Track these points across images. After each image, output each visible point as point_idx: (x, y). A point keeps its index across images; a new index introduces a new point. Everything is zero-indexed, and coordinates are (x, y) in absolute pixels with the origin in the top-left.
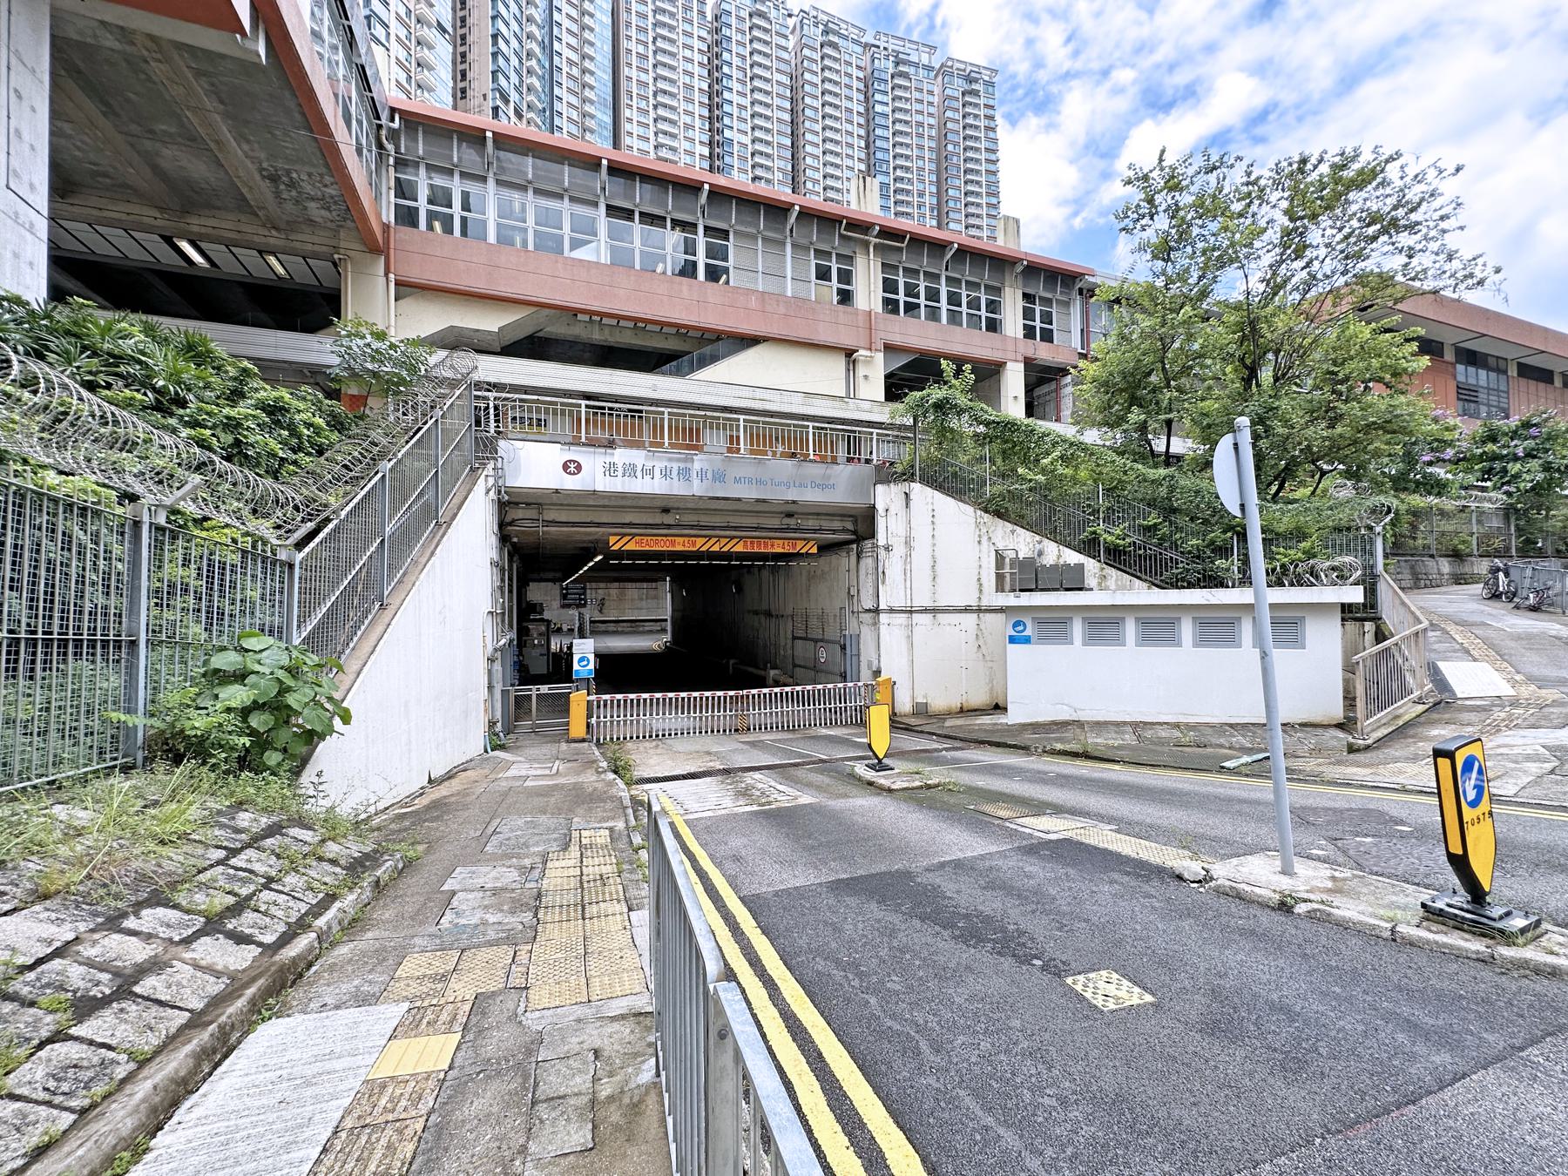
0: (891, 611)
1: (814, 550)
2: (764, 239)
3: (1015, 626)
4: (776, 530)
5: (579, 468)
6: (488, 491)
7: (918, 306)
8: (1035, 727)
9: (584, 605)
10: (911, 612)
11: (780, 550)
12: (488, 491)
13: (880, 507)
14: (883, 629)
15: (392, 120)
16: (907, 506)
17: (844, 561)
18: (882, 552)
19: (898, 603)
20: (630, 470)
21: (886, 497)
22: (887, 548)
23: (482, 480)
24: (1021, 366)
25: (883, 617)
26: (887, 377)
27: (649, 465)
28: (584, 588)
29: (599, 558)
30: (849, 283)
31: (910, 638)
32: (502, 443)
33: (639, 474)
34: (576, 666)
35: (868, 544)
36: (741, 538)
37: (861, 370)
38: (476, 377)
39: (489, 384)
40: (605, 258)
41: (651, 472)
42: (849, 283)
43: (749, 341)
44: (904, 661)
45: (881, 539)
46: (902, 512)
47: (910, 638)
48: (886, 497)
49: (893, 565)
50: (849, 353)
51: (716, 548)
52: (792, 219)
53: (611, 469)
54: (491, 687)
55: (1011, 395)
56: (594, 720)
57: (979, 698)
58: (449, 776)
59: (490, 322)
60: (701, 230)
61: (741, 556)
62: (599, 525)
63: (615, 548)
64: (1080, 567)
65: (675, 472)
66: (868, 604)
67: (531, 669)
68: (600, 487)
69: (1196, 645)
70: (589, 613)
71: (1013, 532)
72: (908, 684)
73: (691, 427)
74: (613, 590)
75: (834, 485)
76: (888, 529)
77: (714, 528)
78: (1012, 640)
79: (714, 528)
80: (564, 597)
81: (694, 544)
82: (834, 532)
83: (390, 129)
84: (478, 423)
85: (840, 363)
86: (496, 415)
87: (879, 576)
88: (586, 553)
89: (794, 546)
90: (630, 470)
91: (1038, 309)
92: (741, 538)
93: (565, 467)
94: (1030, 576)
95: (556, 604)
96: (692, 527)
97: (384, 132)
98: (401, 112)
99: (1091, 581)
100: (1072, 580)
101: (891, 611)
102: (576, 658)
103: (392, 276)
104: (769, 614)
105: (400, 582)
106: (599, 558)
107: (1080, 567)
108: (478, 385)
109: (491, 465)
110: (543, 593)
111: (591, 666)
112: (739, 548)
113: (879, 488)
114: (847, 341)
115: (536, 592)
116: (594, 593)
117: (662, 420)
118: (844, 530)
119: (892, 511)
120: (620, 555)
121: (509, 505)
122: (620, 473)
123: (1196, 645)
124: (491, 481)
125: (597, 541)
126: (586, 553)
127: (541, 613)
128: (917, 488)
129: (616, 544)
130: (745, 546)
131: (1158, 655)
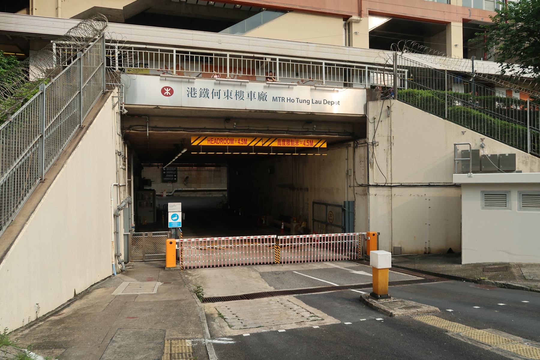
0: (377, 186)
1: (325, 146)
5: (172, 92)
6: (114, 107)
8: (485, 268)
9: (175, 181)
10: (391, 187)
12: (114, 107)
14: (372, 198)
17: (344, 153)
18: (370, 147)
19: (381, 182)
20: (205, 93)
23: (109, 100)
24: (461, 25)
25: (372, 190)
27: (216, 90)
28: (176, 171)
29: (185, 151)
32: (123, 76)
33: (210, 95)
34: (170, 220)
35: (362, 141)
37: (355, 28)
43: (284, 10)
48: (376, 109)
49: (379, 154)
50: (346, 18)
53: (192, 93)
54: (116, 233)
55: (453, 44)
57: (438, 243)
58: (87, 292)
61: (276, 149)
63: (195, 144)
64: (513, 157)
65: (233, 94)
66: (361, 181)
67: (147, 216)
69: (520, 209)
70: (179, 186)
71: (463, 133)
74: (193, 172)
75: (344, 101)
80: (164, 176)
84: (108, 64)
85: (341, 22)
86: (120, 61)
87: (368, 163)
88: (178, 148)
90: (205, 93)
93: (163, 91)
94: (473, 161)
95: (159, 180)
99: (519, 165)
100: (506, 164)
101: (377, 186)
102: (170, 215)
104: (292, 187)
105: (54, 164)
106: (185, 151)
107: (513, 157)
109: (116, 90)
110: (151, 173)
111: (180, 220)
115: (149, 173)
116: (182, 172)
120: (198, 148)
121: (132, 120)
123: (520, 209)
124: (116, 100)
125: (184, 140)
126: (178, 148)
127: (150, 185)
128: (396, 104)
131: (496, 214)
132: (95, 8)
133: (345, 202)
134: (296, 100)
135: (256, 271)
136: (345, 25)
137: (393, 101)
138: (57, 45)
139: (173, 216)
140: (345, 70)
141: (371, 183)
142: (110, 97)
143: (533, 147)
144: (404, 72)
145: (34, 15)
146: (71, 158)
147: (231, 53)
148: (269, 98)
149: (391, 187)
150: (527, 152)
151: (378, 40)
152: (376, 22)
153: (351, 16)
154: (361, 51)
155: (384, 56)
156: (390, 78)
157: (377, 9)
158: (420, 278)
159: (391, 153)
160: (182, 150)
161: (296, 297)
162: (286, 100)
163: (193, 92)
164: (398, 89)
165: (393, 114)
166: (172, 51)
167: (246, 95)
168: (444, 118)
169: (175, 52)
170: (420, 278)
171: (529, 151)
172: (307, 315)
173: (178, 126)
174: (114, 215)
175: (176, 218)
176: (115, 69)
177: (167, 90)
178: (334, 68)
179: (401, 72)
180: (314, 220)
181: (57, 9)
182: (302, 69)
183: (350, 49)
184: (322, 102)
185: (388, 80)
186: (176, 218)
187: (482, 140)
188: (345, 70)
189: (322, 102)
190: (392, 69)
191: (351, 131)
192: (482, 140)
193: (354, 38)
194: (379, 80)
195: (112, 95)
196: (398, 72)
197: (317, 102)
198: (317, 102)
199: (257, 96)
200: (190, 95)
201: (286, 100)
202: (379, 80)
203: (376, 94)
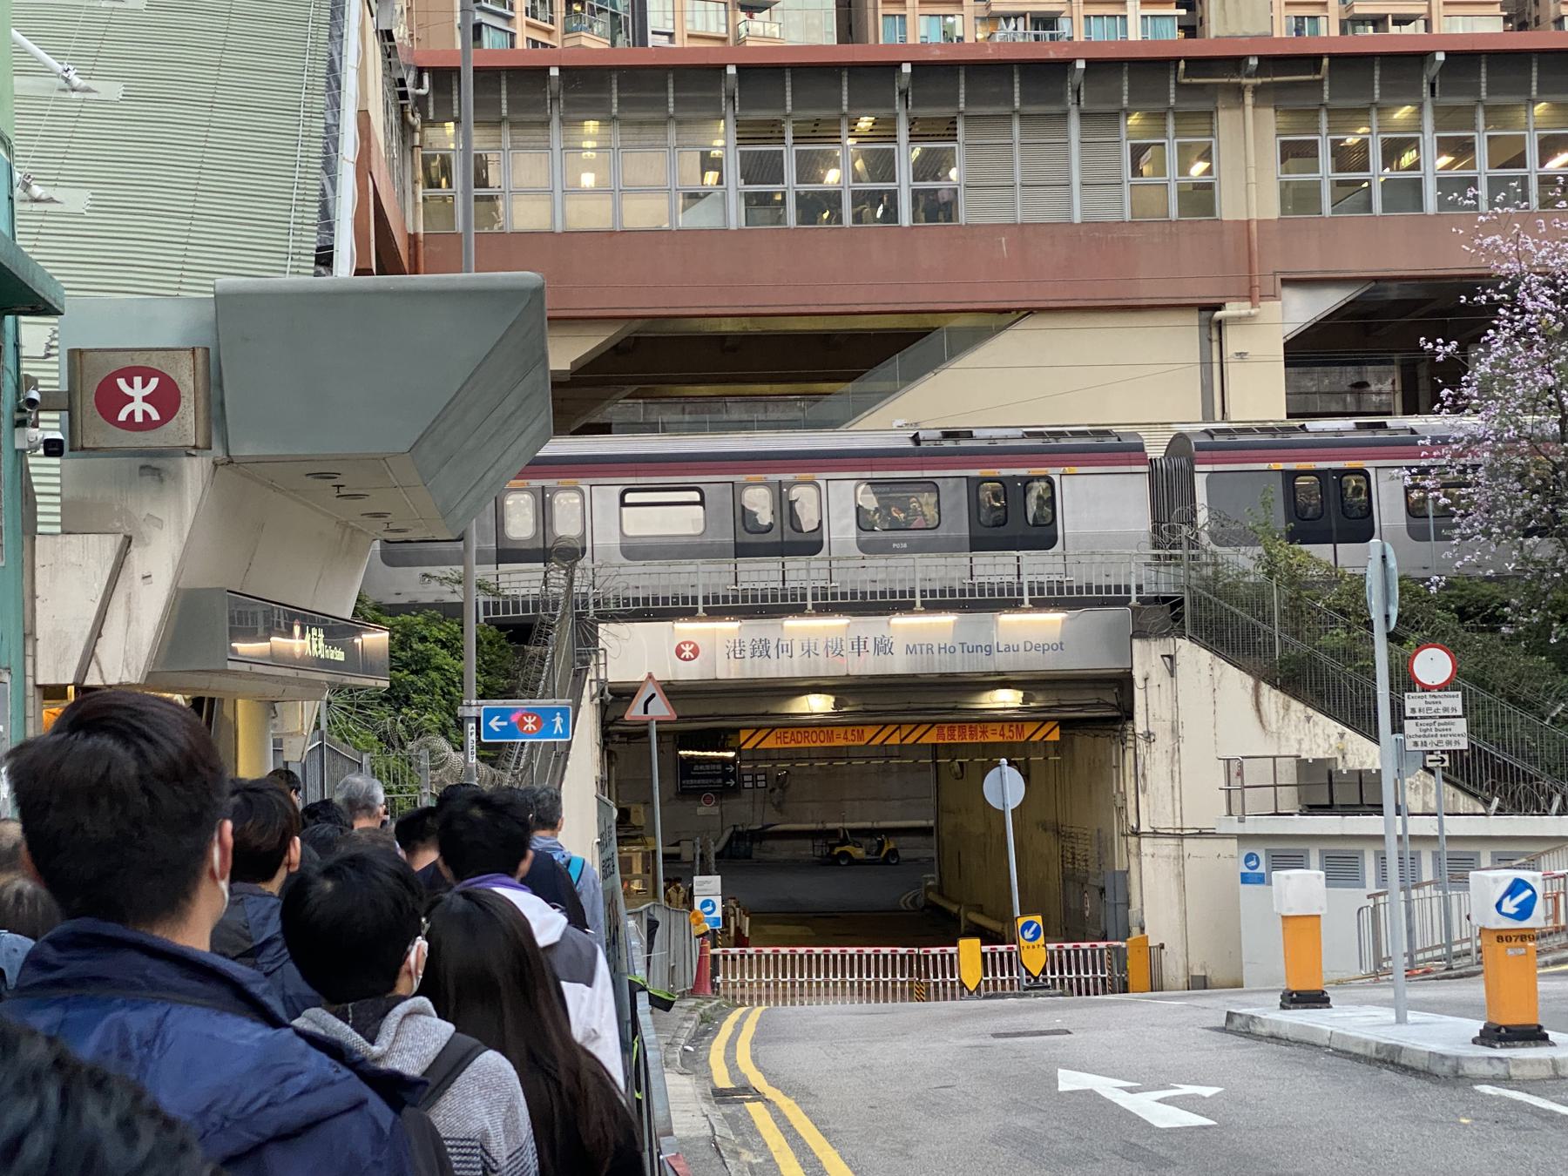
0: (1155, 834)
1: (1055, 736)
2: (1021, 116)
3: (1246, 861)
10: (1182, 837)
13: (1138, 675)
15: (419, 84)
18: (1141, 743)
19: (1165, 823)
21: (1146, 659)
26: (1285, 345)
31: (1181, 876)
33: (773, 652)
36: (933, 723)
37: (1234, 340)
43: (1031, 311)
44: (1175, 914)
45: (1140, 724)
46: (1166, 681)
47: (1181, 876)
48: (1146, 659)
51: (895, 740)
52: (1077, 78)
56: (719, 979)
62: (724, 717)
68: (722, 674)
72: (1180, 950)
76: (1149, 706)
78: (1245, 879)
79: (887, 713)
83: (418, 97)
92: (933, 723)
97: (410, 102)
98: (429, 69)
101: (1155, 834)
112: (931, 738)
113: (1136, 643)
114: (1204, 292)
118: (1099, 705)
119: (1153, 682)
122: (748, 654)
134: (959, 648)
137: (1179, 641)
139: (705, 904)
146: (228, 421)
147: (802, 573)
149: (1182, 837)
152: (1303, 310)
157: (1312, 266)
165: (1179, 670)
173: (710, 712)
175: (709, 909)
177: (687, 649)
186: (709, 909)
187: (1342, 736)
192: (1342, 736)
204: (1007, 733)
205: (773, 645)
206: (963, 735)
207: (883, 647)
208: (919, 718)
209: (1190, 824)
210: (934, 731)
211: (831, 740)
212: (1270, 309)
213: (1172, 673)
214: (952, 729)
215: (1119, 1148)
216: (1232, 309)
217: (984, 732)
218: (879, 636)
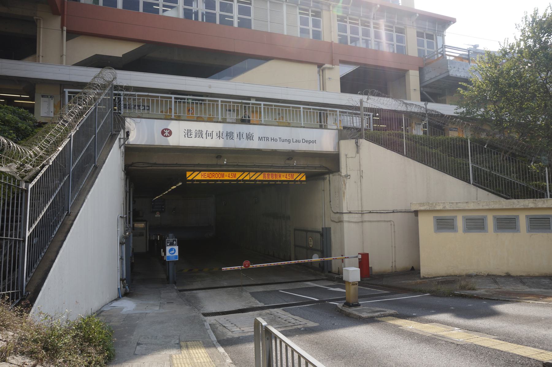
4: (282, 167)
7: (358, 39)
11: (284, 179)
12: (120, 147)
16: (358, 152)
19: (354, 207)
22: (347, 176)
23: (117, 142)
26: (341, 78)
30: (319, 27)
33: (204, 136)
37: (327, 74)
38: (115, 83)
39: (122, 87)
40: (181, 15)
41: (211, 135)
42: (319, 27)
43: (267, 59)
45: (343, 172)
48: (347, 147)
50: (320, 66)
55: (412, 88)
59: (118, 50)
60: (310, 11)
63: (190, 178)
69: (495, 231)
73: (245, 110)
75: (324, 140)
76: (347, 165)
77: (246, 166)
81: (235, 176)
82: (315, 168)
85: (315, 69)
89: (292, 177)
91: (348, 26)
96: (234, 166)
103: (65, 28)
106: (180, 184)
108: (116, 88)
117: (260, 108)
122: (193, 136)
128: (364, 143)
129: (191, 176)
130: (264, 177)
132: (97, 55)
133: (322, 228)
135: (246, 291)
136: (319, 72)
138: (69, 92)
140: (320, 113)
141: (345, 211)
142: (118, 139)
143: (475, 179)
144: (369, 115)
145: (41, 62)
148: (256, 138)
150: (470, 183)
151: (348, 85)
152: (347, 69)
153: (324, 64)
154: (334, 95)
155: (353, 99)
156: (358, 120)
158: (386, 292)
159: (361, 185)
160: (178, 183)
161: (283, 310)
162: (270, 139)
163: (189, 133)
164: (365, 129)
166: (171, 98)
167: (235, 135)
168: (403, 155)
169: (173, 98)
170: (386, 292)
171: (471, 183)
172: (293, 321)
174: (120, 243)
176: (120, 113)
177: (167, 132)
178: (310, 112)
179: (367, 115)
180: (296, 246)
181: (62, 56)
182: (282, 110)
183: (324, 92)
184: (301, 141)
185: (356, 122)
186: (173, 252)
188: (320, 113)
189: (301, 141)
190: (359, 112)
191: (330, 163)
193: (328, 84)
194: (349, 122)
195: (119, 137)
196: (364, 115)
197: (297, 141)
198: (297, 141)
199: (245, 136)
200: (186, 136)
201: (270, 139)
202: (349, 122)
203: (346, 133)
204: (288, 177)
205: (204, 133)
206: (272, 177)
207: (250, 137)
208: (258, 169)
209: (366, 208)
210: (262, 175)
211: (223, 177)
212: (337, 67)
213: (358, 152)
214: (268, 175)
215: (44, 109)
216: (327, 65)
217: (280, 176)
218: (248, 133)
